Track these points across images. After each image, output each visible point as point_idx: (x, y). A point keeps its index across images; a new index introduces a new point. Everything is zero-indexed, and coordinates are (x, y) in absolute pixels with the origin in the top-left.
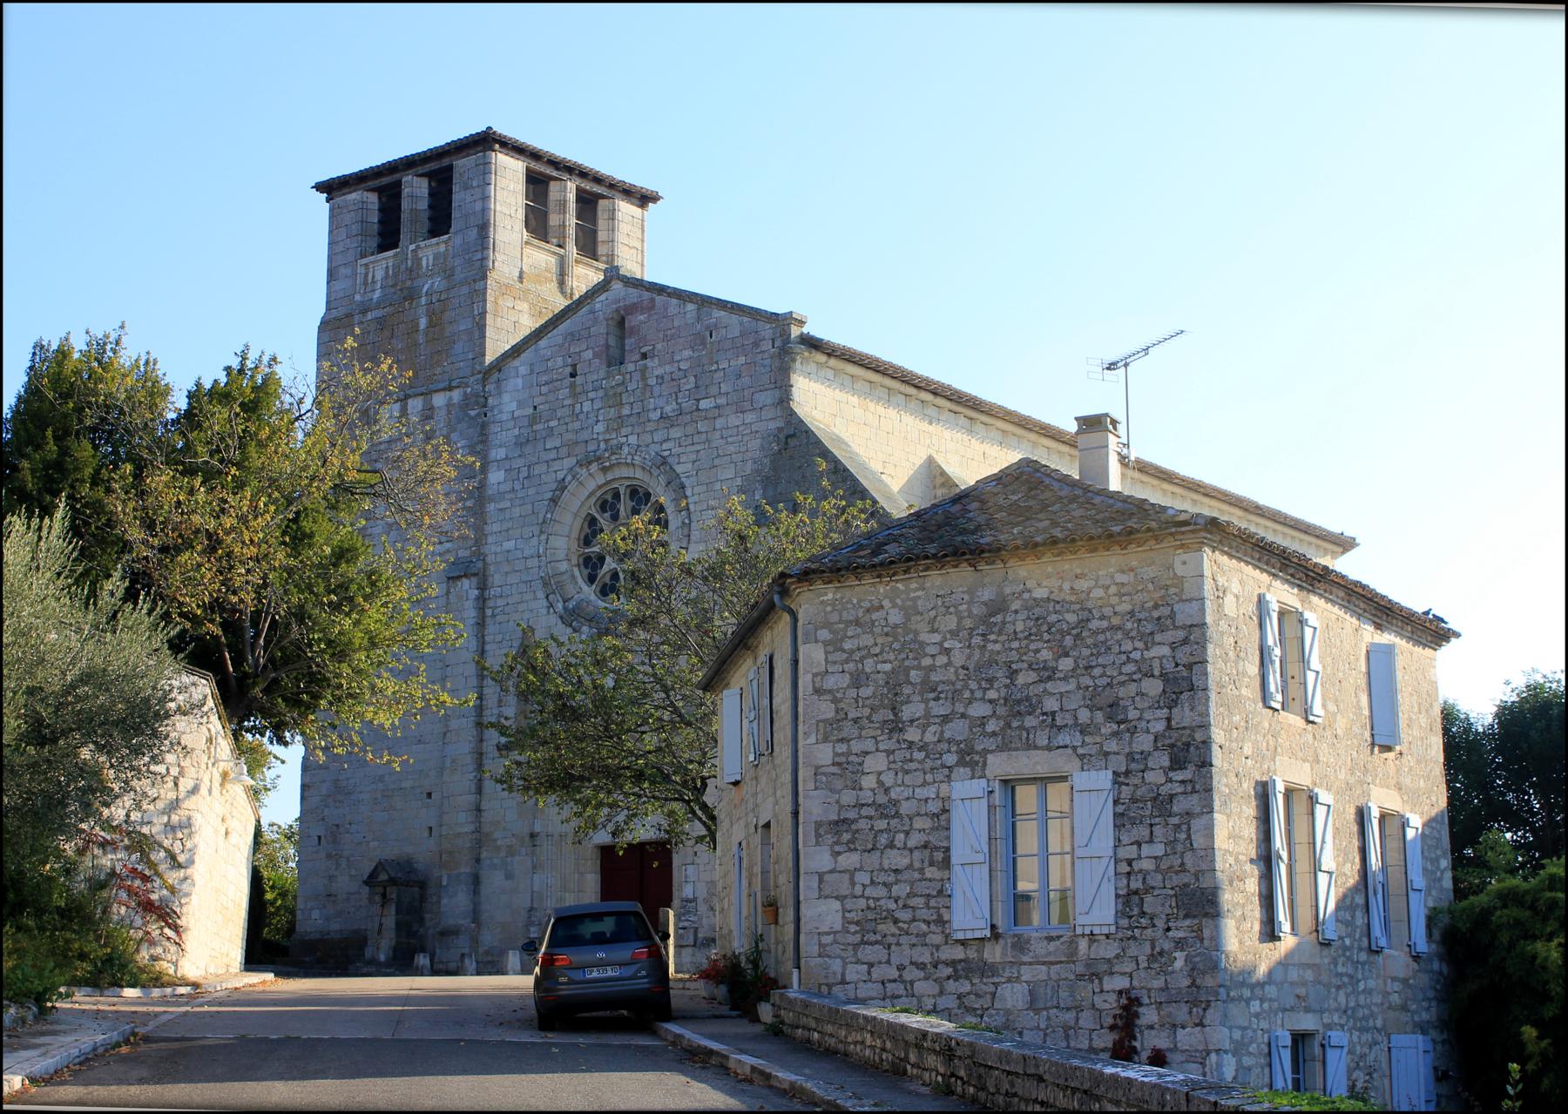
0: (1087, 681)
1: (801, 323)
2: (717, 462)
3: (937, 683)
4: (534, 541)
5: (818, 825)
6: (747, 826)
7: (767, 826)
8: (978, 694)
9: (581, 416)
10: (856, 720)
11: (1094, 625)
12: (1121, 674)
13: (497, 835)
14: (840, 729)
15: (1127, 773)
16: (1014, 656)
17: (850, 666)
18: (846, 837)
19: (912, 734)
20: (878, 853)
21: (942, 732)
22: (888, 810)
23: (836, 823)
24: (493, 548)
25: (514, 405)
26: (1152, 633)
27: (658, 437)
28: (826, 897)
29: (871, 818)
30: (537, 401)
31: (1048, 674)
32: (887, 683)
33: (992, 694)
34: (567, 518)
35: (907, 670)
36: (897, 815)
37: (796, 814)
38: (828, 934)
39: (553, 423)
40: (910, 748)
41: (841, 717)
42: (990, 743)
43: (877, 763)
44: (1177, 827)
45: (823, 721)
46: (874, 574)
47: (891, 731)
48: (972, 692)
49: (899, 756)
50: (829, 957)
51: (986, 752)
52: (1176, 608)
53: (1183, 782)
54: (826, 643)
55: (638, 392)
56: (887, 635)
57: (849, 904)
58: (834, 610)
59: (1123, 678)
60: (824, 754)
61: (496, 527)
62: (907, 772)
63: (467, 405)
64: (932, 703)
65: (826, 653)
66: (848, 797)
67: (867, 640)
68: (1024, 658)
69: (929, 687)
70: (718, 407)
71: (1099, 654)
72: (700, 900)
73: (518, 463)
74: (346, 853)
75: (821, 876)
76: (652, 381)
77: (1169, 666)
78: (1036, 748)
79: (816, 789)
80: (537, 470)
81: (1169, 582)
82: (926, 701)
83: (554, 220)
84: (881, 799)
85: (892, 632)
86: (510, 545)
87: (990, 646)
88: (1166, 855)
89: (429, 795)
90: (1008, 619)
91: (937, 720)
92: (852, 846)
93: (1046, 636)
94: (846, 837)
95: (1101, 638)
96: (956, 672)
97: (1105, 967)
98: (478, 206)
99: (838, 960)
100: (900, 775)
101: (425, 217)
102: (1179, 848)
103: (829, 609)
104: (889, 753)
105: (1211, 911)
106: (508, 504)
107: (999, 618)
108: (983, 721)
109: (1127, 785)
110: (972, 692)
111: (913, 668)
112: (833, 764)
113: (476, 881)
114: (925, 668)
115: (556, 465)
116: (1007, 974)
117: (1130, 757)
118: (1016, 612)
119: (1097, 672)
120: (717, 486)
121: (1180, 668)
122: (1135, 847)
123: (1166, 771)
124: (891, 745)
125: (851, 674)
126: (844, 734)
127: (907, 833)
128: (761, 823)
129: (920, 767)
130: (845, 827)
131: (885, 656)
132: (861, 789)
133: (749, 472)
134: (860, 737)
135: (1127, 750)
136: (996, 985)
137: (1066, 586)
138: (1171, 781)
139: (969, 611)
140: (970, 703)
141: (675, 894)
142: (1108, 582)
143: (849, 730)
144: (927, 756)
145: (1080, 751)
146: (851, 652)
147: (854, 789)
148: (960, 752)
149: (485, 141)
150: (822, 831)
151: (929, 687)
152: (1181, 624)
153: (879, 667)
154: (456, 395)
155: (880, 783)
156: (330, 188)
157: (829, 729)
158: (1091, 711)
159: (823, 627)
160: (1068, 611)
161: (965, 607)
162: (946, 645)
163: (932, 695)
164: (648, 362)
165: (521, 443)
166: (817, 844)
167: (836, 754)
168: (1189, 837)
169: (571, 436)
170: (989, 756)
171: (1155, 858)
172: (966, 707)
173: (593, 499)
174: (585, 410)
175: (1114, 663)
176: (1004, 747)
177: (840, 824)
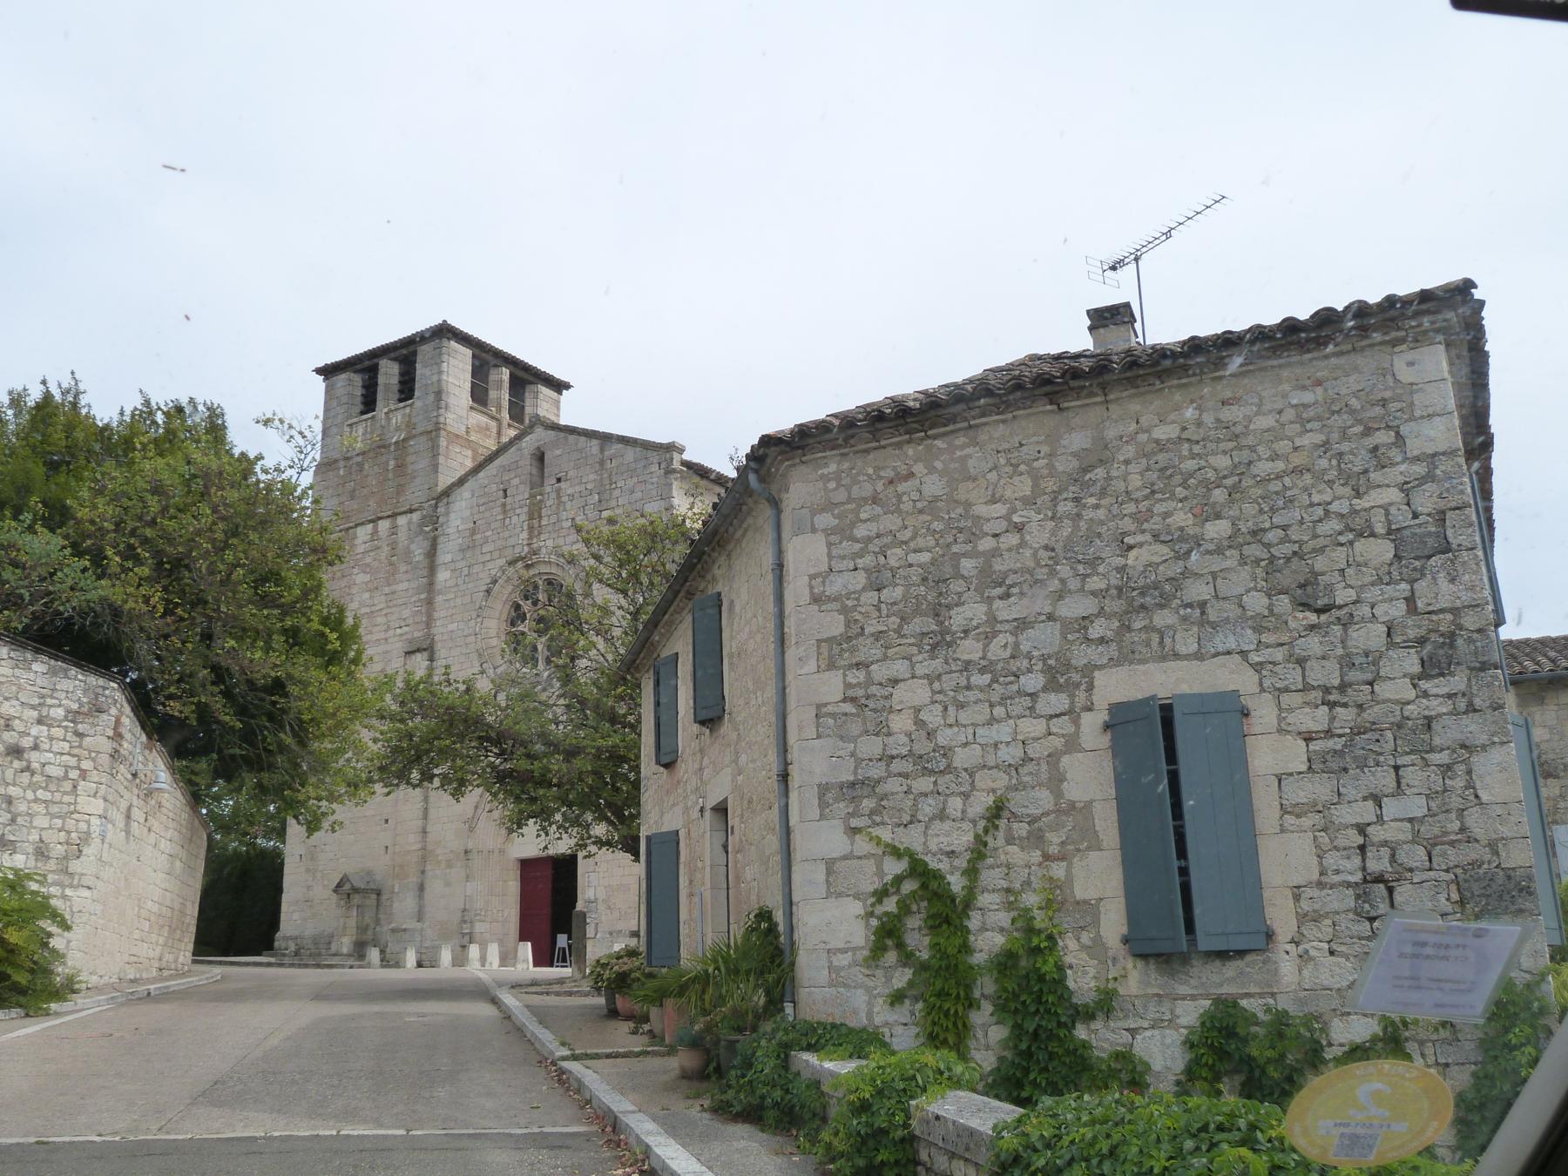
1: (681, 451)
3: (1005, 575)
4: (472, 623)
5: (823, 789)
6: (686, 810)
7: (721, 810)
8: (1073, 584)
10: (877, 636)
12: (1315, 536)
13: (439, 851)
14: (853, 650)
15: (1343, 687)
16: (1128, 524)
17: (868, 560)
18: (868, 804)
19: (970, 649)
20: (920, 827)
21: (1017, 644)
23: (853, 785)
24: (441, 630)
25: (459, 522)
26: (1366, 471)
28: (839, 895)
29: (906, 776)
32: (924, 579)
33: (1096, 583)
34: (499, 606)
36: (949, 769)
37: (784, 777)
38: (844, 951)
39: (488, 534)
40: (966, 669)
42: (1094, 654)
43: (914, 693)
44: (1447, 769)
45: (825, 641)
46: (902, 430)
47: (934, 647)
48: (1063, 581)
49: (948, 682)
50: (845, 985)
52: (1404, 430)
53: (1450, 696)
54: (828, 532)
55: (554, 507)
56: (921, 512)
58: (839, 485)
59: (1321, 542)
60: (831, 687)
61: (443, 614)
62: (961, 706)
64: (998, 604)
65: (829, 545)
66: (871, 746)
67: (891, 522)
68: (1145, 526)
71: (1273, 510)
72: (600, 901)
74: (321, 868)
75: (830, 865)
76: (565, 499)
77: (1402, 517)
78: (1177, 656)
79: (819, 737)
80: (475, 569)
81: (1388, 394)
82: (990, 600)
83: (493, 394)
84: (923, 747)
85: (931, 506)
86: (453, 626)
87: (1088, 514)
88: (1431, 814)
89: (387, 821)
90: (1114, 473)
91: (1007, 627)
92: (878, 819)
93: (1180, 492)
94: (868, 804)
95: (1275, 486)
96: (1035, 554)
97: (1335, 1003)
98: (435, 378)
99: (860, 992)
100: (952, 710)
101: (396, 388)
102: (1455, 802)
103: (832, 485)
104: (931, 678)
105: (1528, 905)
107: (1100, 473)
109: (1345, 705)
110: (1063, 581)
111: (964, 555)
112: (844, 700)
113: (421, 888)
114: (983, 553)
115: (490, 565)
116: (1151, 1015)
117: (1347, 662)
118: (1127, 462)
119: (1271, 536)
121: (1422, 519)
122: (1370, 803)
123: (1415, 680)
125: (866, 570)
126: (860, 657)
127: (966, 796)
128: (712, 801)
129: (981, 696)
130: (866, 791)
131: (920, 542)
132: (889, 734)
134: (885, 658)
135: (1340, 651)
136: (1133, 1032)
137: (1208, 419)
138: (1426, 694)
139: (1050, 466)
140: (1061, 598)
141: (579, 896)
142: (1278, 406)
143: (868, 650)
144: (995, 680)
145: (1254, 658)
146: (869, 540)
147: (877, 735)
148: (1048, 671)
149: (444, 332)
150: (829, 797)
151: (994, 583)
152: (1416, 453)
153: (912, 558)
154: (416, 516)
155: (920, 723)
156: (328, 372)
157: (836, 649)
158: (1269, 596)
159: (823, 510)
160: (1214, 453)
161: (1042, 462)
162: (1016, 519)
163: (999, 591)
164: (562, 485)
166: (822, 817)
167: (848, 686)
168: (1470, 785)
170: (1096, 673)
171: (1411, 820)
172: (1054, 605)
175: (1301, 522)
176: (1126, 658)
177: (854, 788)
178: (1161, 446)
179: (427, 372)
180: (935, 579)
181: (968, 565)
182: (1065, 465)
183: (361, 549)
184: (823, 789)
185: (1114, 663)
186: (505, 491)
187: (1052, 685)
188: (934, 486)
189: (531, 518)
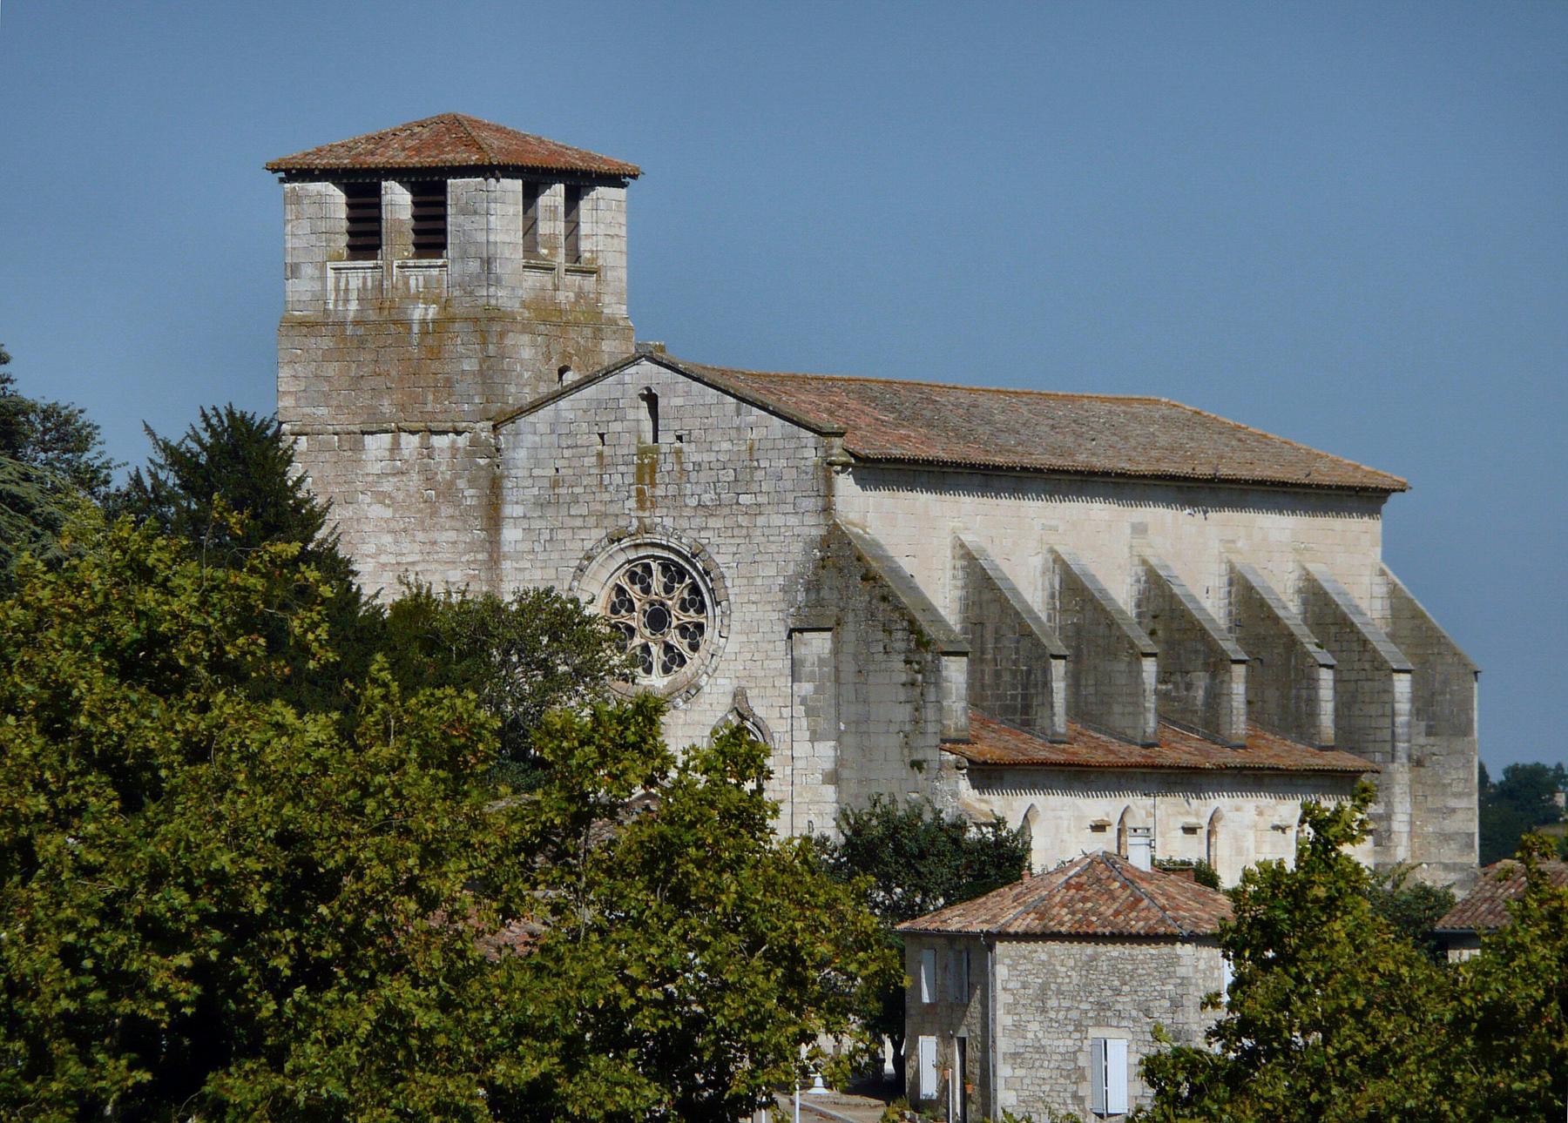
0: (1135, 997)
2: (758, 558)
5: (1005, 1054)
19: (1052, 1015)
22: (1040, 1049)
23: (1014, 1054)
27: (697, 522)
30: (559, 464)
31: (1117, 992)
33: (1091, 999)
35: (1049, 983)
36: (1044, 1052)
41: (1016, 1003)
43: (1034, 1026)
49: (1046, 1024)
54: (1008, 966)
57: (1020, 1093)
63: (475, 452)
66: (1020, 1042)
67: (1029, 967)
69: (1059, 992)
70: (759, 505)
77: (1173, 994)
85: (1043, 963)
108: (1086, 1012)
115: (583, 534)
120: (759, 582)
133: (791, 573)
143: (1020, 1009)
151: (1059, 992)
165: (541, 504)
173: (623, 571)
174: (614, 483)
176: (1098, 1025)
177: (1015, 1055)
178: (1113, 958)
179: (467, 223)
180: (1044, 988)
181: (1053, 986)
182: (1084, 958)
183: (377, 468)
184: (1005, 1054)
186: (602, 436)
187: (1076, 1030)
188: (1044, 957)
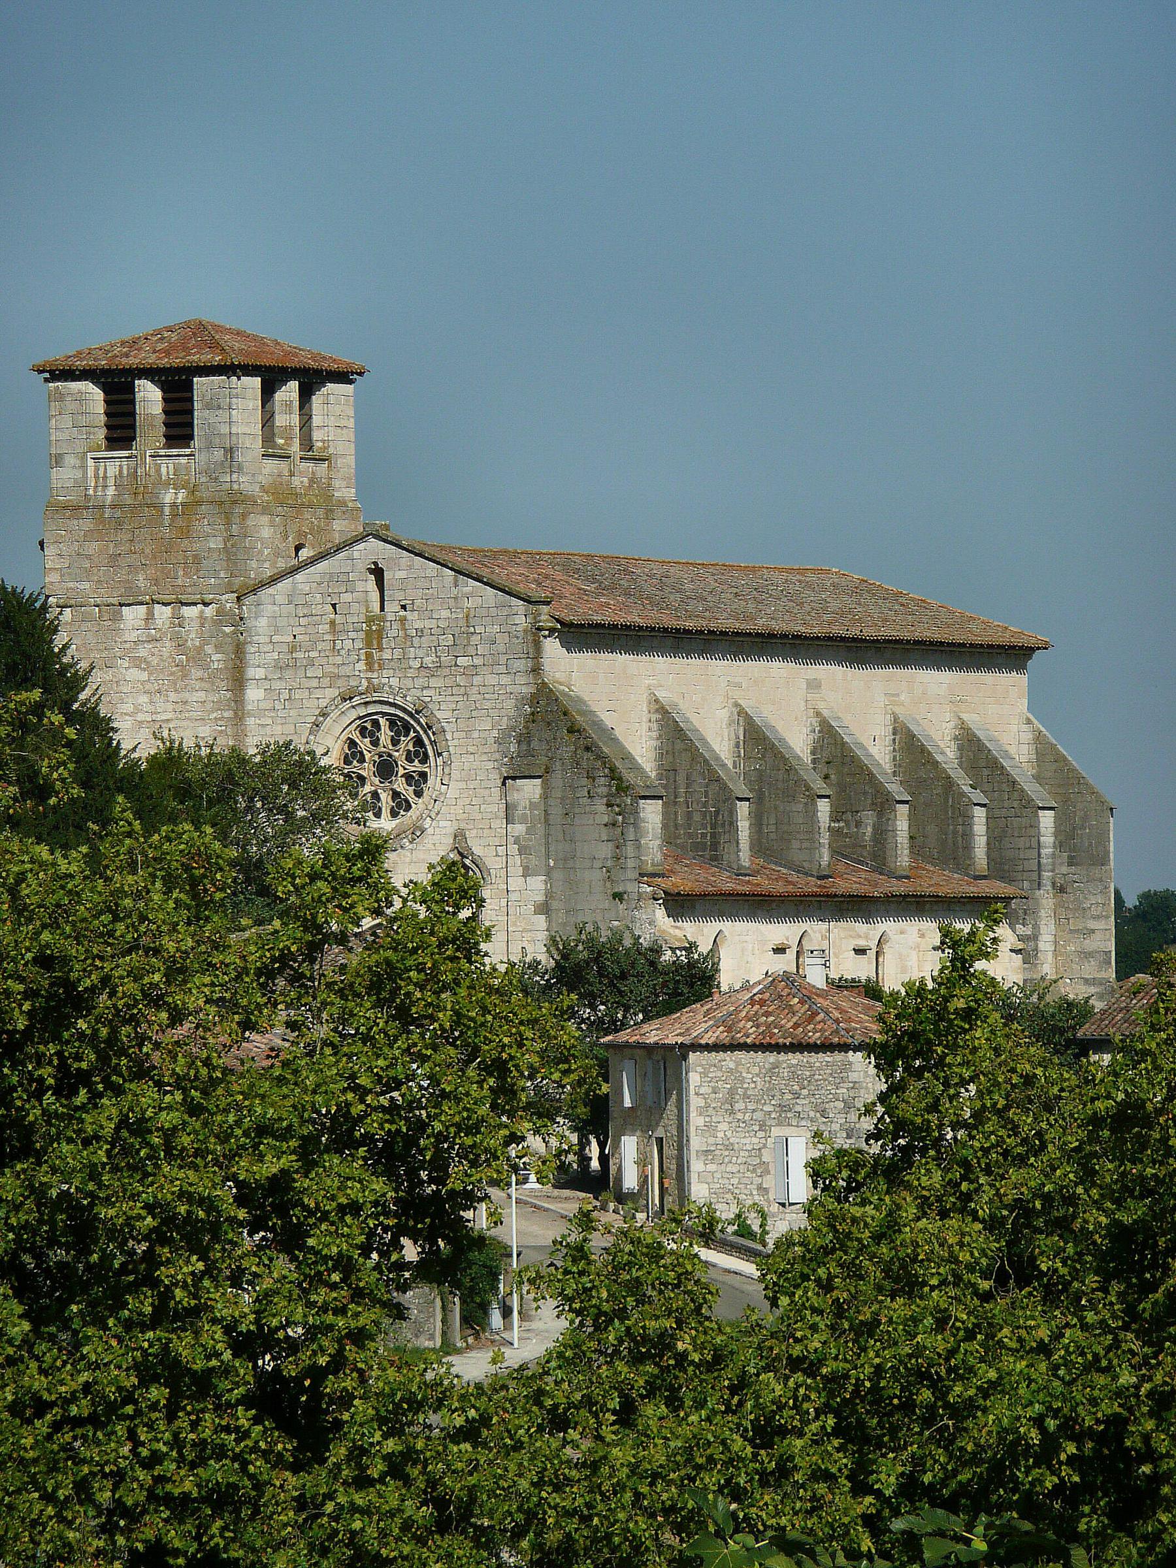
2: (474, 714)
9: (343, 652)
11: (817, 1077)
19: (740, 1116)
22: (729, 1147)
27: (420, 682)
30: (296, 631)
31: (797, 1096)
39: (313, 654)
43: (723, 1126)
51: (771, 1126)
67: (719, 1074)
69: (746, 1096)
73: (277, 685)
80: (297, 695)
85: (731, 1071)
106: (269, 721)
120: (476, 735)
124: (730, 1119)
143: (711, 1111)
151: (746, 1096)
165: (280, 667)
169: (330, 669)
173: (354, 726)
176: (779, 1124)
185: (777, 1125)
186: (334, 606)
188: (732, 1065)
189: (369, 644)
